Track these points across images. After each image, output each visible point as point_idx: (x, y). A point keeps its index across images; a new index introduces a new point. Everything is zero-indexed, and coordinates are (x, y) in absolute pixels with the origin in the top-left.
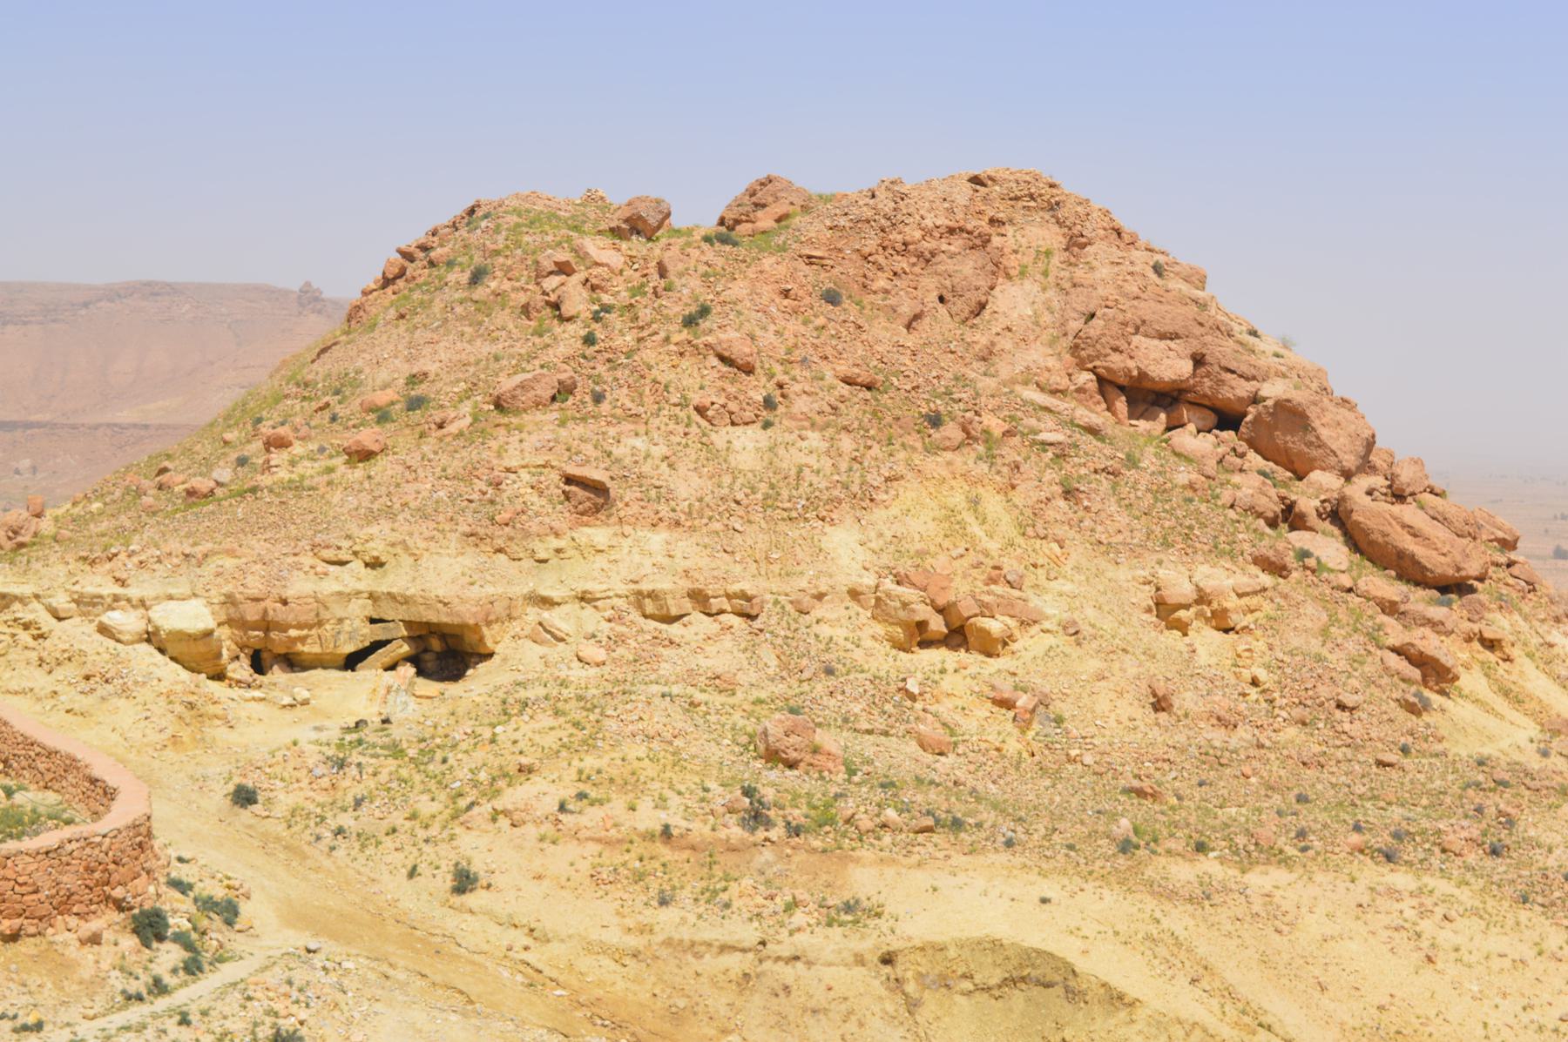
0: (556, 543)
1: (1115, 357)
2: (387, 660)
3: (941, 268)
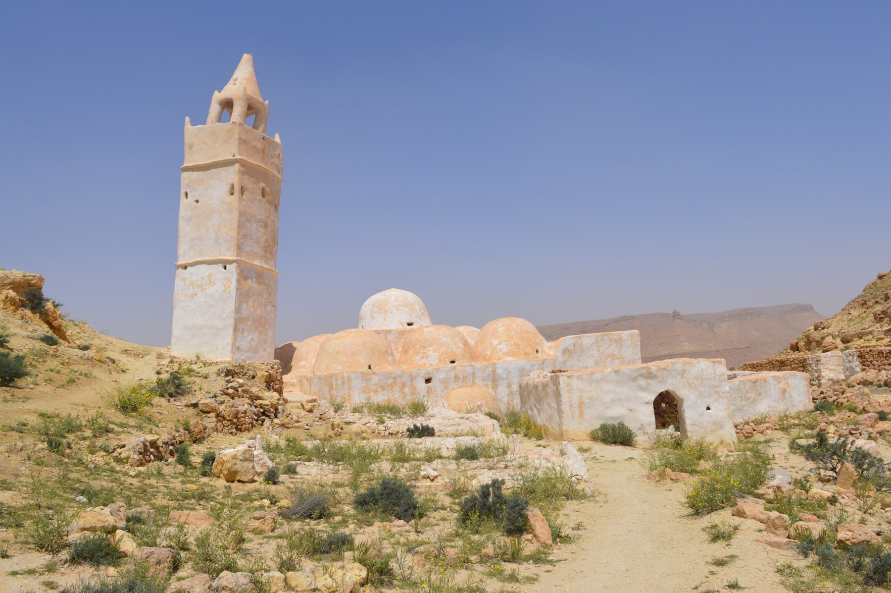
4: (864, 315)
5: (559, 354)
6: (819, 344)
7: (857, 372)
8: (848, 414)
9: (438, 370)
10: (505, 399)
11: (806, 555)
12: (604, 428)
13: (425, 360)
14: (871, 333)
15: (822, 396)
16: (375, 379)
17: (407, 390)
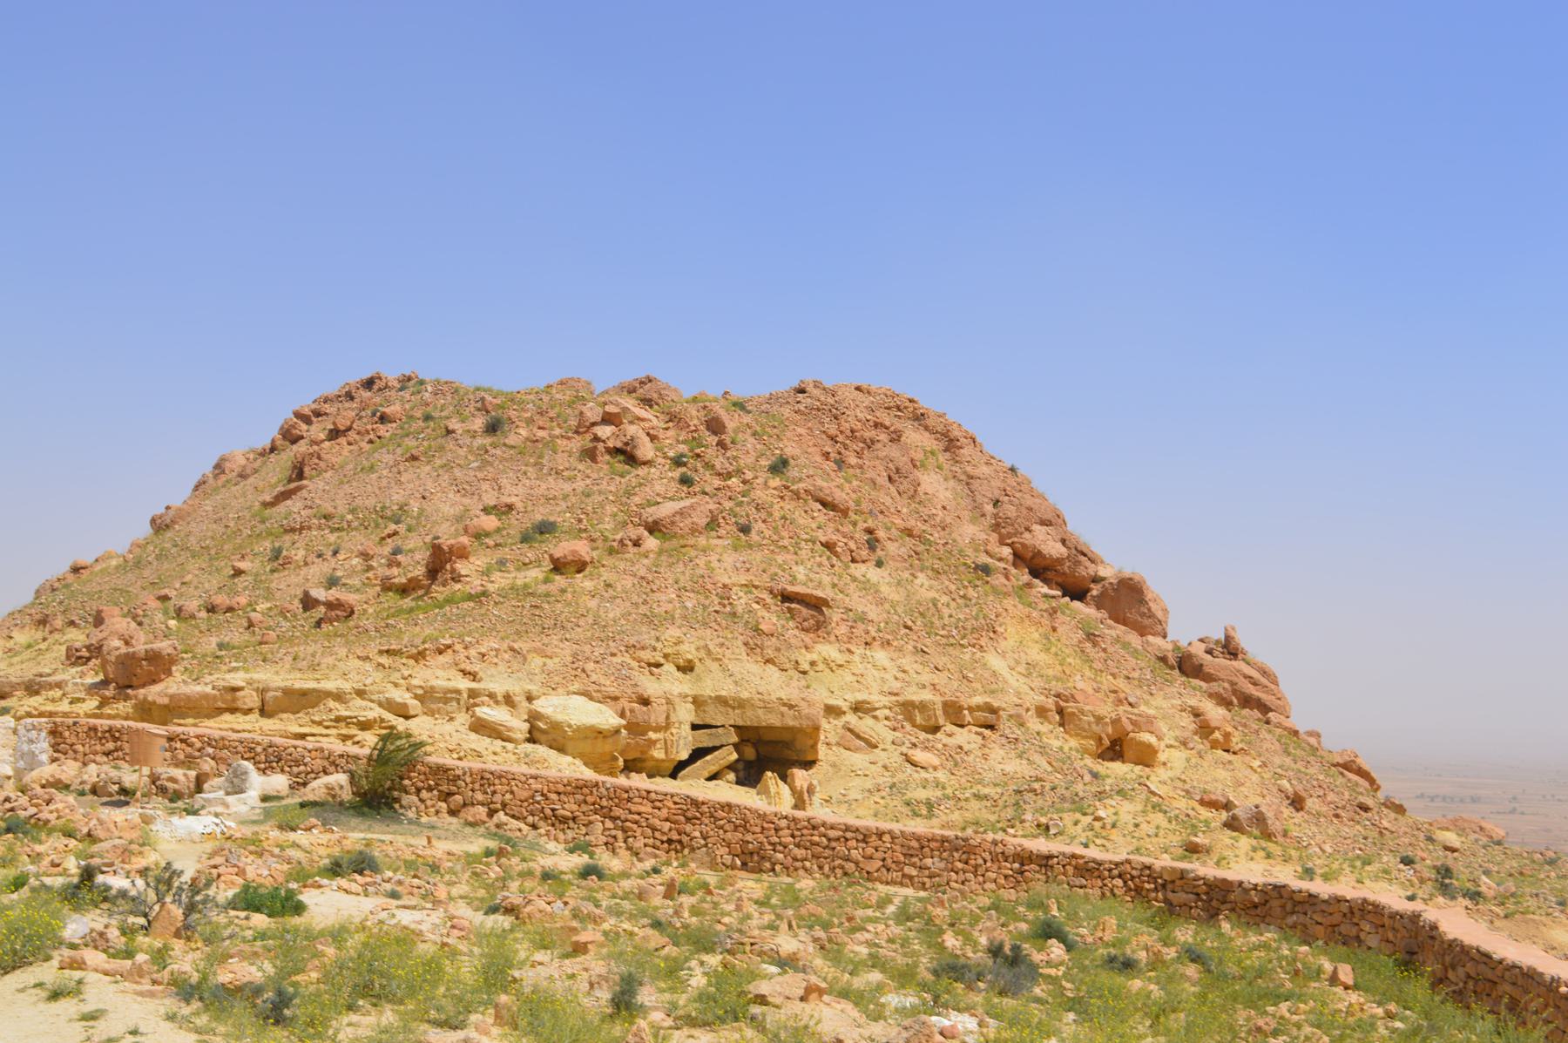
1: (1027, 535)
2: (714, 769)
3: (882, 454)
4: (43, 646)
7: (41, 764)
8: (65, 841)
11: (188, 1003)
14: (59, 685)
15: (8, 805)
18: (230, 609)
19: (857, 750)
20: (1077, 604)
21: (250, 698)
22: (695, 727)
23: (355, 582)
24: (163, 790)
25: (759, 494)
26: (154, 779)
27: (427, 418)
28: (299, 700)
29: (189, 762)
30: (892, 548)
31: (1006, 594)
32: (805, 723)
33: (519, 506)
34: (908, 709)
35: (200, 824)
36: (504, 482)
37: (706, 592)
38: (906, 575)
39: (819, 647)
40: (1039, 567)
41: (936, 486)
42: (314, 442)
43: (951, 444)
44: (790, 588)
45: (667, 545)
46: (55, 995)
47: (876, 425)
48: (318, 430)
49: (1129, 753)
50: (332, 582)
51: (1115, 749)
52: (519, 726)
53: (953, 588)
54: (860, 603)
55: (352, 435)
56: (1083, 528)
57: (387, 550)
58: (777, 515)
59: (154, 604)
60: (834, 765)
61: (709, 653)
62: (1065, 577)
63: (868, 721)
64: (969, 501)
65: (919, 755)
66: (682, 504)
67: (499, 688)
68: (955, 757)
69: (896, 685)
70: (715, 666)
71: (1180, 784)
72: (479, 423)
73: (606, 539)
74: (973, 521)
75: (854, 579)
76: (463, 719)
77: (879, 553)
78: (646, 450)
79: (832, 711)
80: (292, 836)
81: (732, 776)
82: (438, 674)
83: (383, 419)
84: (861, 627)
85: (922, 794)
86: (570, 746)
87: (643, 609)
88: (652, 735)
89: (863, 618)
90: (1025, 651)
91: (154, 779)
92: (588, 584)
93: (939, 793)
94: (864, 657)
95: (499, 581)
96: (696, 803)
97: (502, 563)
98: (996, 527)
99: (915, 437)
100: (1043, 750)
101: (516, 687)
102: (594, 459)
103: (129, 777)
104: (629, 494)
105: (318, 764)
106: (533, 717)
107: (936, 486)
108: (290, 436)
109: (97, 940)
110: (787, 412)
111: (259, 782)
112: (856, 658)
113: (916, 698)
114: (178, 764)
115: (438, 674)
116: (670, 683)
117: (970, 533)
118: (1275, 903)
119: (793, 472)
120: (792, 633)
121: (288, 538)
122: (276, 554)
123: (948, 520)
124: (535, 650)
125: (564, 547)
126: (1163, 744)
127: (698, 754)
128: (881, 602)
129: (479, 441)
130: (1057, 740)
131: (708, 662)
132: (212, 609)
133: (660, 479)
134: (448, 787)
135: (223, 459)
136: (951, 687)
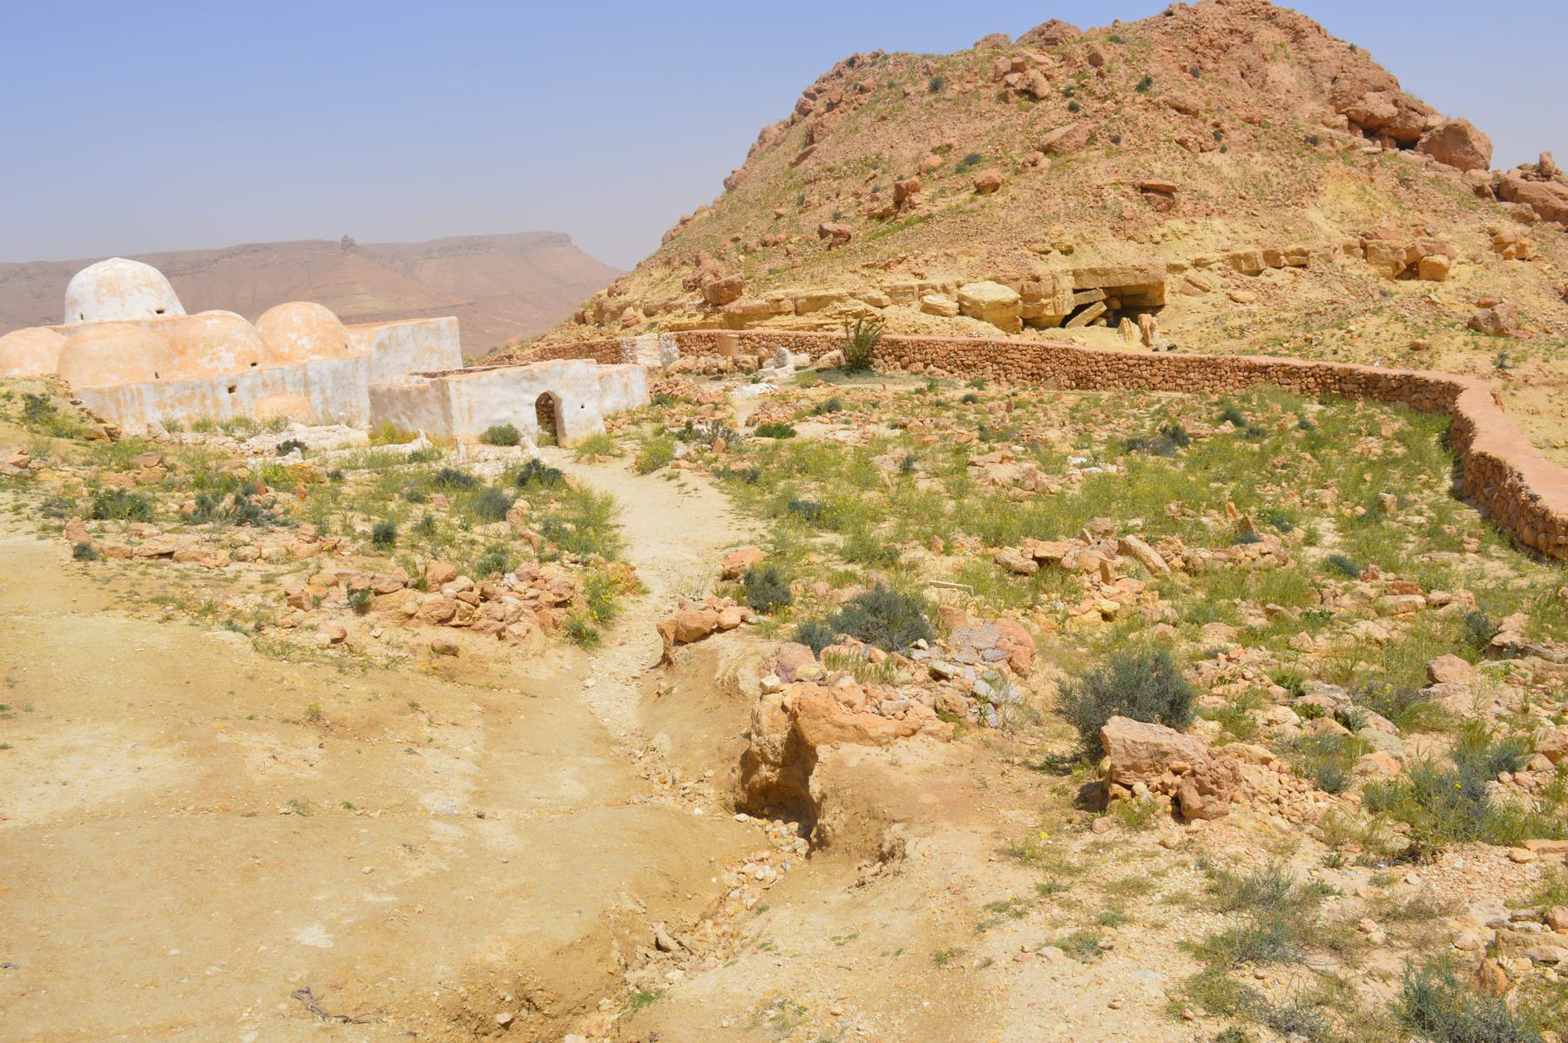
0: (1161, 231)
1: (1360, 103)
2: (1091, 318)
3: (1235, 56)
5: (373, 349)
6: (617, 314)
9: (242, 375)
10: (320, 407)
12: (492, 430)
13: (216, 363)
14: (681, 306)
16: (170, 391)
17: (208, 402)
18: (776, 243)
19: (1194, 294)
20: (1406, 154)
21: (788, 305)
22: (1075, 291)
23: (851, 214)
24: (741, 369)
25: (1128, 111)
26: (735, 363)
27: (891, 86)
28: (817, 303)
29: (753, 351)
30: (1234, 135)
31: (1329, 159)
32: (1152, 281)
33: (956, 144)
34: (1236, 260)
35: (757, 389)
36: (945, 128)
37: (1083, 193)
38: (1245, 156)
39: (1169, 222)
40: (1372, 128)
41: (1282, 74)
42: (818, 115)
43: (1297, 35)
44: (1147, 182)
45: (1058, 161)
46: (670, 479)
47: (1231, 32)
48: (819, 105)
49: (1423, 272)
50: (836, 217)
51: (1412, 269)
52: (951, 305)
53: (1283, 160)
54: (1203, 184)
55: (843, 106)
56: (1413, 86)
57: (870, 189)
58: (1141, 125)
59: (730, 245)
60: (1176, 307)
61: (1084, 238)
62: (1395, 132)
63: (1205, 272)
64: (1310, 82)
65: (1239, 294)
66: (1068, 128)
67: (938, 282)
68: (1269, 294)
69: (1227, 244)
70: (1088, 248)
71: (1463, 292)
72: (925, 85)
73: (1015, 162)
74: (1314, 98)
75: (1201, 165)
76: (916, 304)
77: (1224, 140)
78: (1044, 88)
79: (1175, 268)
80: (808, 391)
81: (1104, 322)
82: (900, 278)
83: (862, 90)
84: (1203, 202)
85: (1237, 322)
86: (985, 315)
87: (1038, 213)
88: (1044, 301)
89: (1205, 196)
90: (1346, 200)
91: (735, 363)
92: (1000, 200)
93: (1249, 320)
94: (1204, 226)
95: (942, 204)
96: (1047, 350)
97: (942, 191)
98: (1333, 100)
99: (1268, 35)
100: (1343, 279)
101: (948, 279)
102: (1007, 101)
103: (722, 364)
104: (1032, 124)
105: (825, 345)
106: (961, 299)
107: (1282, 74)
108: (803, 111)
109: (687, 457)
110: (1156, 35)
111: (792, 360)
112: (1198, 227)
113: (1242, 252)
114: (748, 352)
115: (900, 278)
116: (1059, 262)
117: (1310, 109)
118: (1406, 387)
119: (1155, 88)
120: (1149, 214)
121: (807, 187)
122: (801, 201)
123: (1292, 101)
124: (963, 252)
125: (981, 175)
126: (1454, 262)
127: (1079, 309)
128: (1221, 180)
129: (927, 99)
130: (1357, 268)
131: (1084, 245)
132: (765, 244)
133: (1054, 109)
134: (899, 352)
135: (763, 132)
136: (1271, 239)
